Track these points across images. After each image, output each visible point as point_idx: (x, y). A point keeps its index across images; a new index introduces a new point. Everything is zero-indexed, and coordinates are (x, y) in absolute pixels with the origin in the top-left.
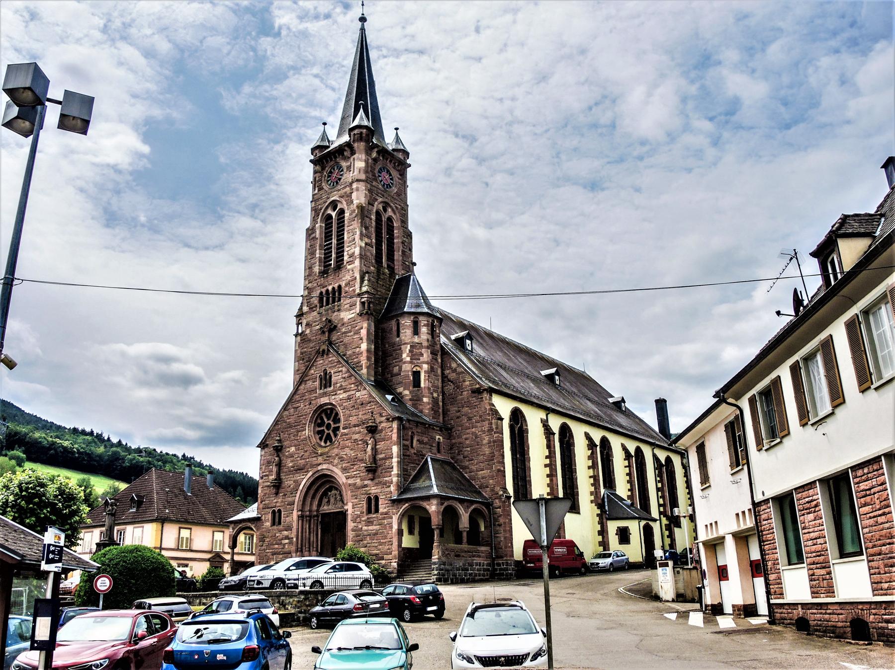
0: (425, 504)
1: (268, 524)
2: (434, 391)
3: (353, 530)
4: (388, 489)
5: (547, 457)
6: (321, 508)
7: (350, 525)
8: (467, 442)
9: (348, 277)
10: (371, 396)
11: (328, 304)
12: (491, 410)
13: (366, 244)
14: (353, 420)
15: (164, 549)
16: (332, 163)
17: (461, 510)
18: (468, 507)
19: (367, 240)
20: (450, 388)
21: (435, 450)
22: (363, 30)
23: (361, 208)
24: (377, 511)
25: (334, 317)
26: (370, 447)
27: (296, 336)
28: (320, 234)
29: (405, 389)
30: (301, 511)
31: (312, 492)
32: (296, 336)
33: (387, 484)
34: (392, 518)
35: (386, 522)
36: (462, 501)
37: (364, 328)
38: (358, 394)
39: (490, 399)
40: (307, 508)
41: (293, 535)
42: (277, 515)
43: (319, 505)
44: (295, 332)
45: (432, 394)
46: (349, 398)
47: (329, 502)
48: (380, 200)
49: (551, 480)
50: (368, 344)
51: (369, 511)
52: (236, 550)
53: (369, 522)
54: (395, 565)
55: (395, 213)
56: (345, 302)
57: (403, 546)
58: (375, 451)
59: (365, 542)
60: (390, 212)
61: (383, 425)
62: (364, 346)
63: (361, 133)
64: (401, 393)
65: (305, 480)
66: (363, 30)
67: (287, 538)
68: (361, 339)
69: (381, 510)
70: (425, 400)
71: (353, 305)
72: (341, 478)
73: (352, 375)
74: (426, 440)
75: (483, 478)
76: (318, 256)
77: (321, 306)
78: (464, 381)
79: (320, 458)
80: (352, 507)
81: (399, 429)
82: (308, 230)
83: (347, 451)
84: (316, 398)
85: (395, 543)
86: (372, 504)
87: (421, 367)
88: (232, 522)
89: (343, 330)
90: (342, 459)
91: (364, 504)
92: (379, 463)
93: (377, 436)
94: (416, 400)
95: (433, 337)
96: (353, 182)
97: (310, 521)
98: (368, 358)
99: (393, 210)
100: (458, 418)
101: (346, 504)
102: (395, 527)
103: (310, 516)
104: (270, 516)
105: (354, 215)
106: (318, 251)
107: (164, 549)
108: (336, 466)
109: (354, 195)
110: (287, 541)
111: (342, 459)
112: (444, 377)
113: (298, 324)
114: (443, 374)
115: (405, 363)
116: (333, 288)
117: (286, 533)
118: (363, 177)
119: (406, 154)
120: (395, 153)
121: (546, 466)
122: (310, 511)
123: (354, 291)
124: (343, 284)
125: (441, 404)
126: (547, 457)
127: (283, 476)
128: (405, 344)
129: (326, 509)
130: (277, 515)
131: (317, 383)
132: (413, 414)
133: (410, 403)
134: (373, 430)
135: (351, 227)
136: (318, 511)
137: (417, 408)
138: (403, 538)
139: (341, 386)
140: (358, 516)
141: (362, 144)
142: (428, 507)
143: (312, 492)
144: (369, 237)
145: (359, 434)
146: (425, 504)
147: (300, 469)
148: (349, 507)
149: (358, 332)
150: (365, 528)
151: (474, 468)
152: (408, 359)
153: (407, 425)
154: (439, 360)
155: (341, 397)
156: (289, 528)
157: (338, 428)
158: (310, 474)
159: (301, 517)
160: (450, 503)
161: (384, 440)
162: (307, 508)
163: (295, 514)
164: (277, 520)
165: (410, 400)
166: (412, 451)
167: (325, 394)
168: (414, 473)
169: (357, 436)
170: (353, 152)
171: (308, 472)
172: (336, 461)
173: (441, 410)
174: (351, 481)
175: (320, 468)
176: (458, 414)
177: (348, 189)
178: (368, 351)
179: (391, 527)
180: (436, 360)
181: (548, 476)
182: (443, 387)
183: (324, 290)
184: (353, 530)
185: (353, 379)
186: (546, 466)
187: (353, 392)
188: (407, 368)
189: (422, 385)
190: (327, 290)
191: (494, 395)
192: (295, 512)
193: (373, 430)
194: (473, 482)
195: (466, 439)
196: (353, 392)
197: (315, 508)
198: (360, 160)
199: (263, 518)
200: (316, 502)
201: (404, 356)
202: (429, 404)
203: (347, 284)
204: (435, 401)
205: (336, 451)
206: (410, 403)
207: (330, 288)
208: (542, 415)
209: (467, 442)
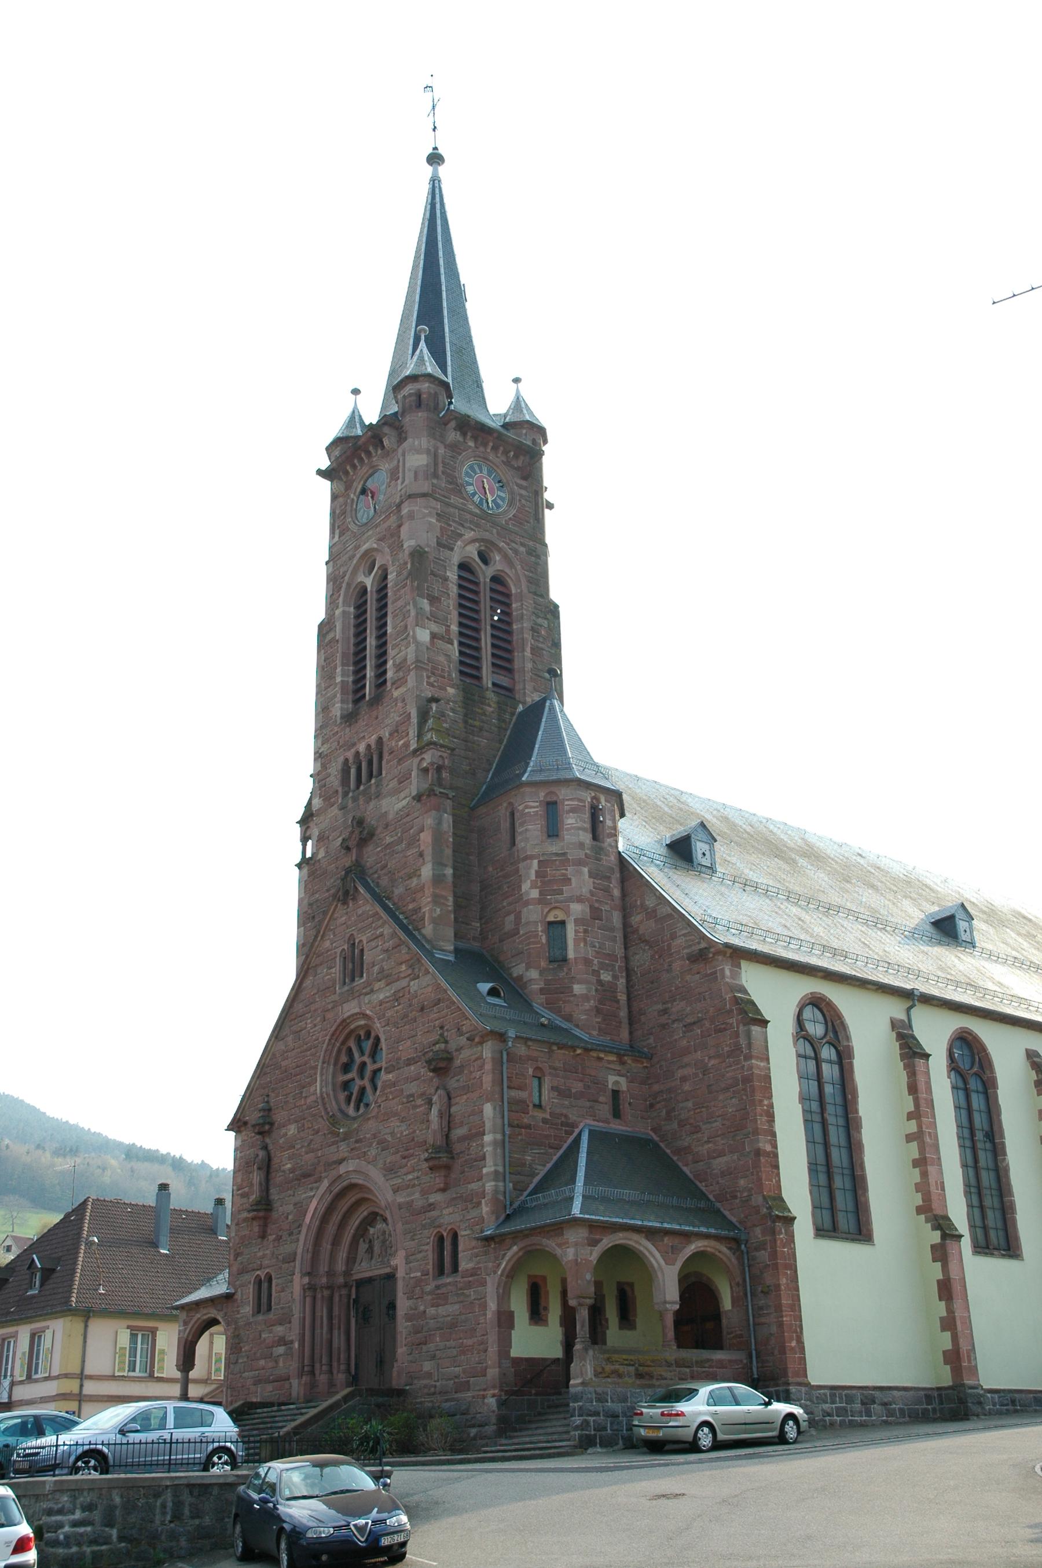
0: (550, 1244)
1: (247, 1310)
2: (603, 966)
3: (409, 1318)
4: (474, 1213)
5: (910, 1116)
6: (357, 1268)
7: (403, 1305)
8: (687, 1087)
9: (395, 717)
10: (438, 987)
11: (359, 782)
12: (736, 1001)
13: (434, 636)
14: (406, 1049)
15: (91, 1377)
16: (365, 469)
17: (651, 1252)
18: (675, 1250)
19: (435, 627)
20: (642, 958)
21: (605, 1109)
22: (435, 185)
23: (418, 554)
24: (455, 1269)
25: (371, 811)
26: (434, 1111)
27: (299, 866)
28: (343, 631)
29: (528, 967)
30: (309, 1274)
31: (331, 1229)
32: (299, 866)
33: (473, 1200)
34: (484, 1284)
35: (472, 1293)
36: (650, 1233)
37: (433, 827)
38: (414, 985)
39: (736, 975)
40: (323, 1268)
41: (293, 1335)
42: (265, 1285)
43: (351, 1260)
44: (298, 858)
45: (596, 973)
46: (396, 998)
47: (370, 1250)
48: (469, 535)
49: (924, 1174)
50: (438, 863)
51: (440, 1271)
52: (192, 1374)
53: (440, 1298)
54: (492, 1401)
55: (511, 564)
56: (390, 769)
57: (515, 1353)
58: (448, 1121)
59: (431, 1346)
60: (498, 564)
61: (465, 1054)
62: (427, 871)
63: (419, 395)
64: (520, 978)
65: (315, 1201)
66: (435, 185)
67: (282, 1341)
68: (421, 855)
69: (464, 1265)
70: (578, 989)
71: (404, 779)
72: (383, 1191)
73: (402, 943)
74: (577, 1087)
75: (723, 1174)
76: (339, 679)
77: (345, 794)
78: (674, 937)
79: (343, 1146)
80: (406, 1261)
81: (498, 1062)
82: (321, 626)
83: (394, 1123)
84: (336, 1004)
85: (493, 1349)
86: (445, 1253)
87: (567, 912)
88: (182, 1307)
89: (388, 840)
90: (384, 1145)
91: (429, 1252)
92: (457, 1148)
93: (452, 1083)
94: (556, 993)
95: (595, 838)
96: (402, 502)
97: (331, 1298)
98: (437, 899)
99: (505, 557)
100: (664, 1026)
101: (393, 1255)
102: (492, 1306)
103: (330, 1287)
104: (250, 1290)
105: (405, 573)
106: (339, 670)
107: (91, 1377)
108: (373, 1162)
109: (404, 530)
110: (281, 1350)
111: (384, 1145)
112: (628, 933)
113: (304, 840)
114: (626, 925)
115: (527, 903)
116: (369, 746)
117: (279, 1330)
118: (425, 487)
119: (539, 432)
120: (511, 434)
121: (909, 1138)
122: (331, 1274)
123: (407, 745)
124: (386, 734)
125: (623, 998)
126: (910, 1116)
127: (274, 1194)
128: (526, 858)
129: (365, 1269)
130: (265, 1285)
131: (337, 971)
132: (551, 1027)
133: (542, 998)
134: (441, 1065)
135: (400, 603)
136: (347, 1273)
137: (558, 1011)
138: (514, 1334)
139: (382, 970)
140: (418, 1282)
141: (421, 415)
142: (558, 1251)
143: (331, 1229)
144: (443, 621)
145: (416, 1079)
146: (550, 1244)
147: (306, 1176)
148: (398, 1261)
149: (414, 841)
150: (431, 1311)
151: (704, 1149)
152: (535, 894)
153: (522, 1050)
154: (617, 893)
155: (382, 996)
156: (285, 1320)
157: (376, 1072)
158: (326, 1183)
159: (311, 1289)
160: (620, 1238)
161: (467, 1089)
162: (323, 1268)
163: (298, 1282)
164: (264, 1300)
165: (542, 991)
166: (539, 1115)
167: (352, 995)
168: (542, 1171)
169: (412, 1088)
170: (402, 438)
171: (319, 1180)
172: (373, 1152)
173: (623, 1013)
174: (400, 1199)
175: (342, 1169)
176: (663, 1020)
177: (393, 518)
178: (438, 879)
179: (484, 1306)
180: (607, 890)
181: (916, 1163)
182: (626, 958)
183: (350, 755)
184: (409, 1318)
185: (404, 950)
186: (909, 1138)
187: (403, 983)
188: (533, 915)
189: (571, 954)
190: (358, 753)
191: (744, 964)
192: (297, 1278)
193: (441, 1065)
194: (702, 1186)
195: (684, 1079)
196: (403, 983)
197: (340, 1266)
198: (418, 451)
199: (238, 1296)
200: (342, 1254)
201: (526, 886)
202: (586, 998)
203: (395, 732)
204: (606, 992)
205: (372, 1124)
206: (542, 998)
207: (362, 748)
208: (896, 1009)
209: (687, 1087)
